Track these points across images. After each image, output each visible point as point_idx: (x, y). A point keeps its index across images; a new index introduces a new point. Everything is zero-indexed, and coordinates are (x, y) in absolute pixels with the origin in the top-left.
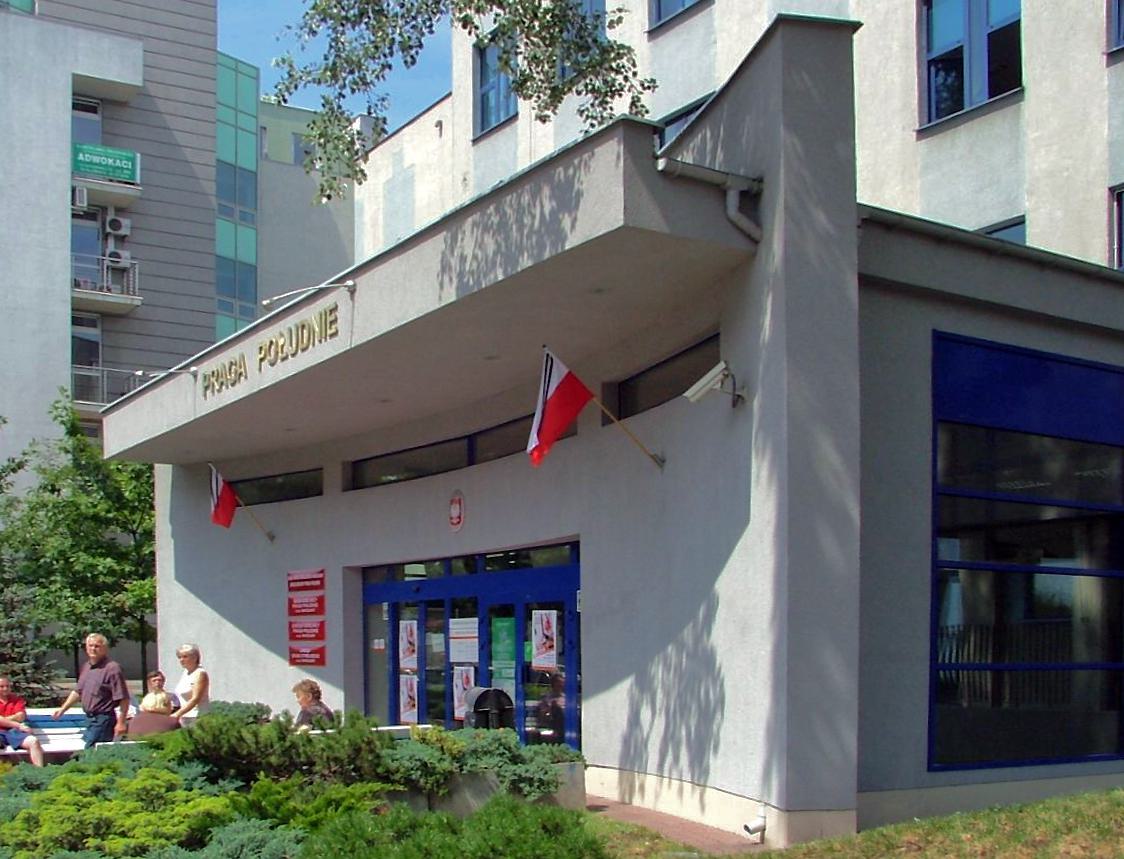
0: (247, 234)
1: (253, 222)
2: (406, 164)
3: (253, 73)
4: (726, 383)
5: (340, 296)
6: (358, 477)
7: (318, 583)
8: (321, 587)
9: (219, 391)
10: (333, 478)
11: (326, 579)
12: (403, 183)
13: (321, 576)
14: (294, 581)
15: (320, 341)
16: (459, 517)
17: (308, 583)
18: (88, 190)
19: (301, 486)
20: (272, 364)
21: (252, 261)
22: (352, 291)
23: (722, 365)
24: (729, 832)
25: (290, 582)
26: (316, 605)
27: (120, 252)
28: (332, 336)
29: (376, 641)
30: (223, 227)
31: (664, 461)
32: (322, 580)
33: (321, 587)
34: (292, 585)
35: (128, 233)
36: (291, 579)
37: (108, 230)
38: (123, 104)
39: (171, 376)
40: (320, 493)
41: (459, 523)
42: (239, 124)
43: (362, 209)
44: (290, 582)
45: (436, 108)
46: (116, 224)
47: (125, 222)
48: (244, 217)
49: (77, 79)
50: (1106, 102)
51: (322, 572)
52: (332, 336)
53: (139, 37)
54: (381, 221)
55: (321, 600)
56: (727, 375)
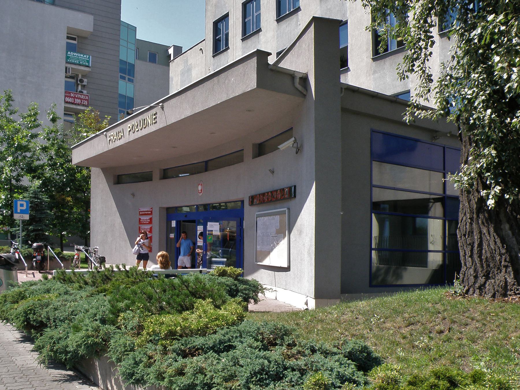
0: (130, 85)
1: (133, 82)
2: (189, 63)
3: (134, 29)
4: (294, 145)
5: (158, 109)
6: (166, 175)
7: (150, 212)
8: (151, 214)
9: (114, 142)
10: (156, 175)
11: (153, 212)
12: (188, 70)
13: (151, 210)
14: (141, 212)
15: (151, 125)
16: (201, 190)
17: (146, 213)
18: (72, 68)
19: (146, 178)
20: (133, 133)
21: (132, 96)
22: (162, 108)
23: (293, 139)
24: (280, 241)
25: (139, 212)
26: (149, 221)
27: (83, 91)
28: (155, 123)
29: (171, 234)
30: (121, 83)
31: (273, 172)
32: (151, 212)
33: (151, 214)
34: (141, 213)
35: (86, 84)
36: (140, 211)
37: (79, 82)
38: (86, 38)
39: (97, 136)
40: (151, 180)
41: (201, 192)
42: (128, 47)
43: (172, 79)
44: (139, 212)
45: (442, 156)
46: (81, 81)
47: (85, 80)
48: (129, 80)
49: (68, 28)
50: (438, 51)
51: (151, 209)
52: (155, 123)
53: (92, 14)
54: (179, 83)
55: (151, 219)
56: (295, 141)
